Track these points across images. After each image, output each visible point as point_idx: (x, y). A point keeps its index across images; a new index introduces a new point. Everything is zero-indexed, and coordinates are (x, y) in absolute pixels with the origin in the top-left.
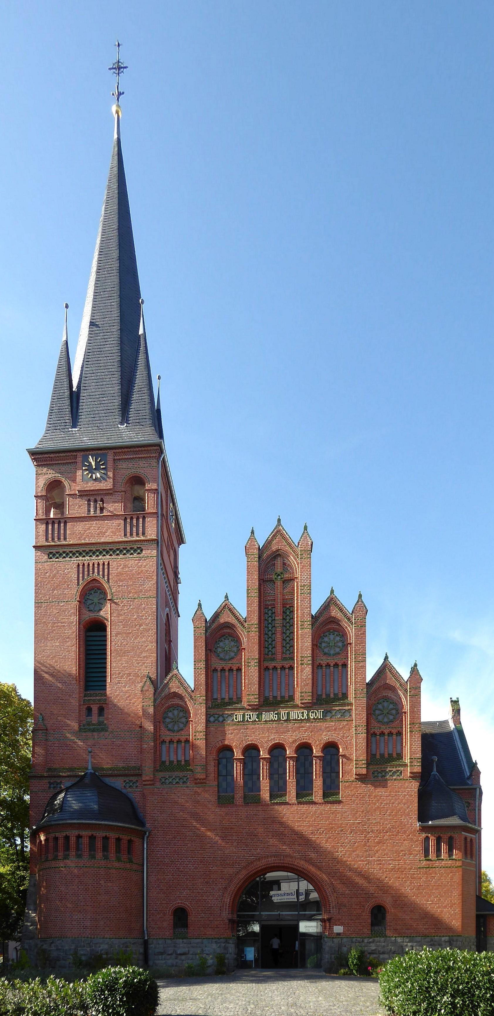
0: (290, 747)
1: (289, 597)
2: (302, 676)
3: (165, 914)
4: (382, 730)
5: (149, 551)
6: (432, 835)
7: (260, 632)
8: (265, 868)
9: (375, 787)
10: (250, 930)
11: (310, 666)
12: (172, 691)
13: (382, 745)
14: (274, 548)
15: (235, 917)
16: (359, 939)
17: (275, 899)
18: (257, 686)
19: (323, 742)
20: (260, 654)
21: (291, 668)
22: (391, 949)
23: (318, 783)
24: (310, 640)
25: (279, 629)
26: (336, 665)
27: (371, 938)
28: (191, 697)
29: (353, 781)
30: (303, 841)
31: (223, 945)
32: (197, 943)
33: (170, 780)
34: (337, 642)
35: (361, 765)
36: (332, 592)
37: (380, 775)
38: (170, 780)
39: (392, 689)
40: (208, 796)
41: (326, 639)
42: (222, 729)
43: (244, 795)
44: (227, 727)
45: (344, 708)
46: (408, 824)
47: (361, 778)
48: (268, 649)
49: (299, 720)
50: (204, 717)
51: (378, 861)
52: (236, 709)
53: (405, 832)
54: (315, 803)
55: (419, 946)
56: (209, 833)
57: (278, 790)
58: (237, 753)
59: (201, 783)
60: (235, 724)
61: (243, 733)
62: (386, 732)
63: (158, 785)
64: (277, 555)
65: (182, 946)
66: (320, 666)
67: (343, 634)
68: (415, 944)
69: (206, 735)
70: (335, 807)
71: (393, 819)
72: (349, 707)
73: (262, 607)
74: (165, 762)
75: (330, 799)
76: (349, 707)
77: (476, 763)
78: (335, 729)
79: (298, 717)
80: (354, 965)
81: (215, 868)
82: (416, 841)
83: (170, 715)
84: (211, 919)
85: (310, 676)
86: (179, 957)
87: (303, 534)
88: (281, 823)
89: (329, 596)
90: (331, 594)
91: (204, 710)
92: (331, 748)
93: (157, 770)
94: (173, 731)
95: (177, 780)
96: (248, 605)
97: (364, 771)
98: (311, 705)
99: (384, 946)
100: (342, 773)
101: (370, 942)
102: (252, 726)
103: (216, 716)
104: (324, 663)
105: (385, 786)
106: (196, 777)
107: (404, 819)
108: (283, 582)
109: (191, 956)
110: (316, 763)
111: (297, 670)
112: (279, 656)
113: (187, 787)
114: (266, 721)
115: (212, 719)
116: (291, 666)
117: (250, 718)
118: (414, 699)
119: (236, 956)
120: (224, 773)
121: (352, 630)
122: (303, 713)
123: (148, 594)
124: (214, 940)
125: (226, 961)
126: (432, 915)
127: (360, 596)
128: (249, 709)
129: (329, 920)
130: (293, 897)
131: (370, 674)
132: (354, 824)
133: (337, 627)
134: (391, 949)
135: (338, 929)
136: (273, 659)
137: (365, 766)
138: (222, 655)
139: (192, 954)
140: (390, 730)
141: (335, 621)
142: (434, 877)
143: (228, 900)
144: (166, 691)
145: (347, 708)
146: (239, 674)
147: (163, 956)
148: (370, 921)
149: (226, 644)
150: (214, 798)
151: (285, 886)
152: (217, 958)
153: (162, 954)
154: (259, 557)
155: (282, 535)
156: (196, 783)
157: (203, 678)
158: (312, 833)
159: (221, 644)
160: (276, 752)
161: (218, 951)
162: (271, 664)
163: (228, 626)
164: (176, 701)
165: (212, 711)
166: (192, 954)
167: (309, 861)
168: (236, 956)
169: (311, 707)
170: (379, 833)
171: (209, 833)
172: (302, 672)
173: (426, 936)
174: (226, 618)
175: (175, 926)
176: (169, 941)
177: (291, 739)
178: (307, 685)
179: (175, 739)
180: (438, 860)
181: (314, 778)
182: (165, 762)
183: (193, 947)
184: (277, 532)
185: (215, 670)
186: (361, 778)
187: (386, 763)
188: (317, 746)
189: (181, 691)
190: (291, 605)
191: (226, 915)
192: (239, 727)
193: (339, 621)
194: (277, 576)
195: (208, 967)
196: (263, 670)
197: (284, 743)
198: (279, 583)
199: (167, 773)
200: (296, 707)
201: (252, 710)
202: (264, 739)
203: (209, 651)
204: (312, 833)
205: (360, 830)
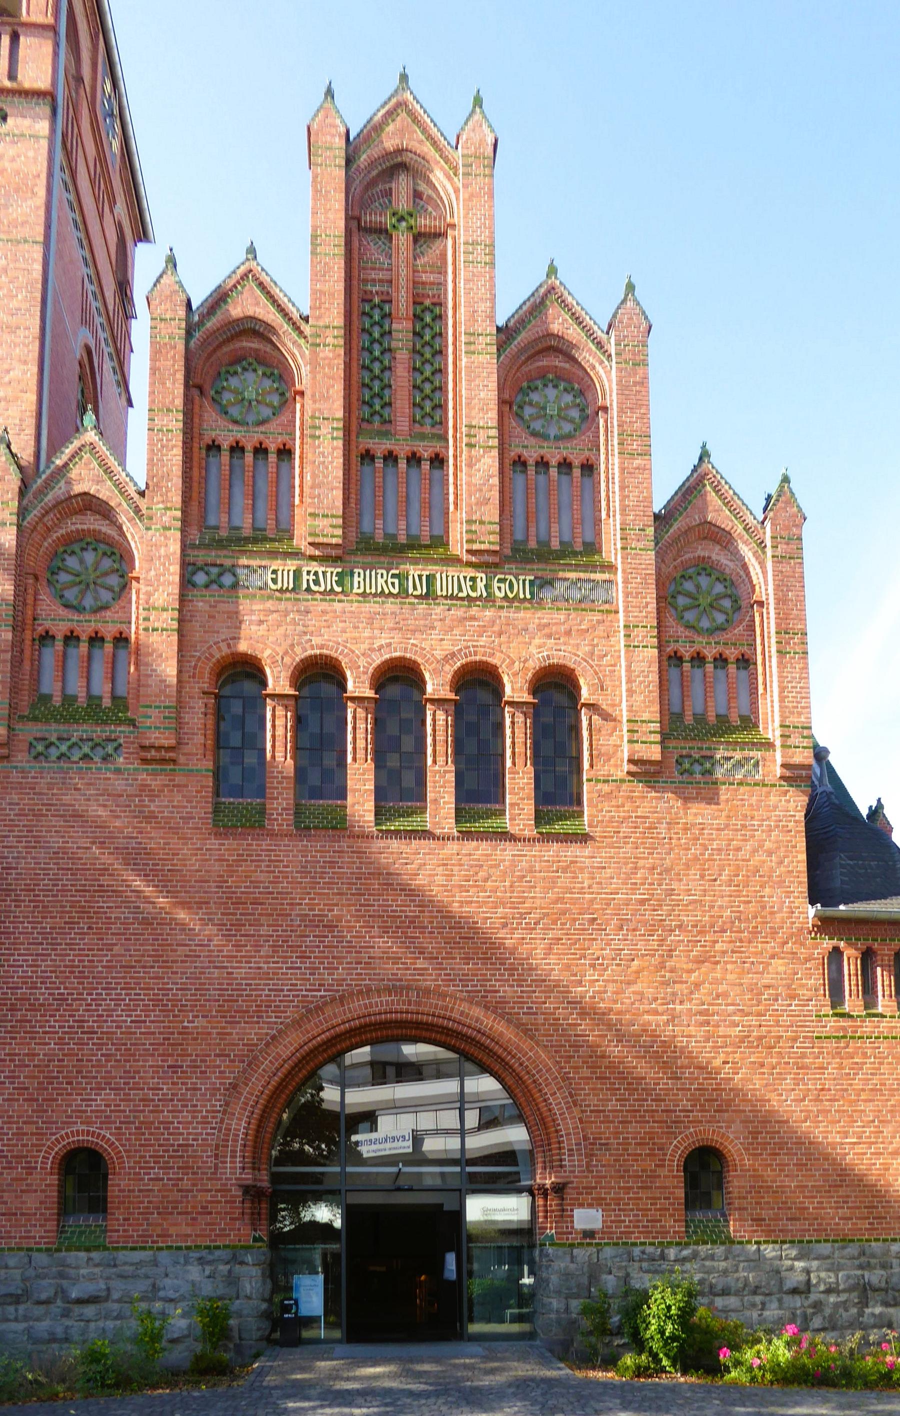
0: (435, 672)
1: (432, 278)
2: (473, 482)
3: (30, 1170)
4: (697, 647)
5: (27, 122)
6: (850, 944)
7: (348, 351)
8: (362, 1027)
9: (686, 800)
10: (307, 1219)
11: (495, 453)
12: (78, 489)
13: (697, 689)
14: (390, 144)
15: (264, 1181)
16: (650, 1249)
17: (366, 1151)
18: (338, 494)
19: (534, 665)
20: (348, 408)
21: (439, 461)
22: (746, 1279)
23: (519, 780)
24: (492, 383)
25: (403, 355)
26: (565, 465)
27: (687, 1244)
28: (137, 510)
29: (622, 781)
30: (466, 939)
31: (223, 1268)
32: (139, 1264)
33: (64, 748)
34: (567, 407)
35: (645, 733)
36: (552, 271)
37: (697, 768)
38: (64, 748)
39: (721, 537)
40: (189, 795)
41: (535, 397)
42: (230, 607)
43: (297, 805)
44: (245, 605)
45: (593, 576)
46: (780, 910)
47: (646, 773)
48: (371, 406)
49: (462, 599)
50: (175, 568)
51: (700, 1013)
52: (273, 554)
53: (774, 932)
54: (513, 838)
55: (828, 1270)
56: (182, 915)
57: (400, 790)
58: (277, 679)
59: (163, 761)
60: (270, 597)
61: (294, 623)
62: (709, 653)
63: (21, 758)
64: (398, 165)
65: (86, 1272)
66: (520, 463)
67: (579, 385)
68: (815, 1264)
69: (181, 621)
70: (573, 851)
71: (738, 893)
72: (606, 576)
73: (355, 297)
74: (50, 697)
75: (557, 828)
76: (606, 576)
77: (876, 812)
78: (568, 633)
79: (460, 589)
80: (666, 1342)
81: (200, 1022)
82: (807, 960)
83: (72, 562)
84: (186, 1184)
85: (495, 481)
86: (77, 1310)
87: (470, 115)
88: (411, 893)
89: (545, 282)
90: (548, 276)
91: (175, 547)
92: (556, 688)
93: (21, 717)
94: (78, 609)
95: (86, 749)
96: (317, 276)
97: (654, 753)
98: (497, 559)
99: (725, 1272)
100: (591, 755)
101: (684, 1260)
102: (324, 606)
103: (215, 571)
104: (531, 456)
105: (712, 799)
106: (147, 743)
107: (773, 896)
108: (415, 240)
109: (116, 1306)
110: (513, 723)
111: (455, 466)
112: (403, 424)
113: (118, 771)
114: (364, 595)
115: (200, 578)
116: (437, 455)
117: (317, 582)
118: (786, 568)
119: (264, 1306)
120: (236, 740)
121: (608, 373)
122: (473, 579)
123: (17, 234)
124: (194, 1255)
125: (232, 1322)
126: (861, 1178)
127: (630, 287)
128: (312, 558)
129: (559, 1189)
130: (406, 1144)
131: (662, 492)
132: (628, 902)
133: (567, 366)
134: (746, 1279)
135: (586, 1218)
136: (386, 434)
137: (658, 738)
138: (235, 412)
139: (119, 1301)
140: (720, 648)
141: (558, 347)
142: (859, 1066)
143: (240, 1125)
144: (59, 491)
145: (598, 576)
146: (284, 465)
147: (22, 1308)
148: (681, 1193)
149: (251, 384)
150: (201, 809)
151: (385, 1123)
152: (201, 1312)
153: (16, 1299)
154: (349, 162)
155: (412, 114)
156: (145, 761)
157: (175, 456)
158: (505, 925)
159: (234, 382)
160: (393, 691)
161: (208, 1289)
162: (380, 446)
163: (255, 329)
164: (92, 523)
165: (202, 556)
166: (119, 1301)
167: (496, 1007)
168: (264, 1306)
169: (496, 565)
170: (700, 932)
171: (182, 915)
172: (470, 465)
173: (846, 1241)
174: (247, 305)
175: (65, 1208)
176: (41, 1259)
177: (439, 649)
178: (487, 501)
179: (85, 630)
180: (870, 1015)
181: (509, 763)
182: (50, 697)
183: (121, 1276)
184: (399, 105)
185: (214, 447)
186: (647, 773)
187: (714, 735)
188: (516, 674)
189: (105, 492)
190: (436, 300)
191: (235, 1171)
192: (282, 606)
193: (574, 346)
194: (399, 221)
195: (173, 1341)
196: (358, 459)
197: (419, 660)
198: (402, 239)
199: (54, 726)
200: (456, 561)
201: (323, 559)
202: (360, 628)
203: (195, 392)
204: (505, 925)
205: (645, 923)
